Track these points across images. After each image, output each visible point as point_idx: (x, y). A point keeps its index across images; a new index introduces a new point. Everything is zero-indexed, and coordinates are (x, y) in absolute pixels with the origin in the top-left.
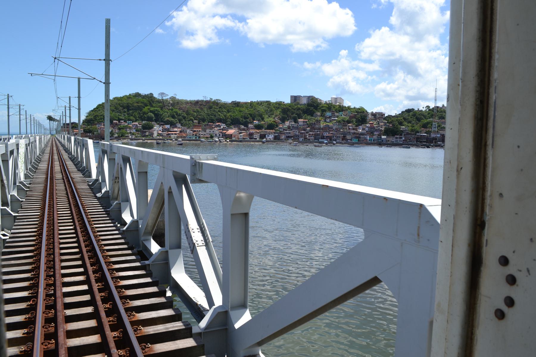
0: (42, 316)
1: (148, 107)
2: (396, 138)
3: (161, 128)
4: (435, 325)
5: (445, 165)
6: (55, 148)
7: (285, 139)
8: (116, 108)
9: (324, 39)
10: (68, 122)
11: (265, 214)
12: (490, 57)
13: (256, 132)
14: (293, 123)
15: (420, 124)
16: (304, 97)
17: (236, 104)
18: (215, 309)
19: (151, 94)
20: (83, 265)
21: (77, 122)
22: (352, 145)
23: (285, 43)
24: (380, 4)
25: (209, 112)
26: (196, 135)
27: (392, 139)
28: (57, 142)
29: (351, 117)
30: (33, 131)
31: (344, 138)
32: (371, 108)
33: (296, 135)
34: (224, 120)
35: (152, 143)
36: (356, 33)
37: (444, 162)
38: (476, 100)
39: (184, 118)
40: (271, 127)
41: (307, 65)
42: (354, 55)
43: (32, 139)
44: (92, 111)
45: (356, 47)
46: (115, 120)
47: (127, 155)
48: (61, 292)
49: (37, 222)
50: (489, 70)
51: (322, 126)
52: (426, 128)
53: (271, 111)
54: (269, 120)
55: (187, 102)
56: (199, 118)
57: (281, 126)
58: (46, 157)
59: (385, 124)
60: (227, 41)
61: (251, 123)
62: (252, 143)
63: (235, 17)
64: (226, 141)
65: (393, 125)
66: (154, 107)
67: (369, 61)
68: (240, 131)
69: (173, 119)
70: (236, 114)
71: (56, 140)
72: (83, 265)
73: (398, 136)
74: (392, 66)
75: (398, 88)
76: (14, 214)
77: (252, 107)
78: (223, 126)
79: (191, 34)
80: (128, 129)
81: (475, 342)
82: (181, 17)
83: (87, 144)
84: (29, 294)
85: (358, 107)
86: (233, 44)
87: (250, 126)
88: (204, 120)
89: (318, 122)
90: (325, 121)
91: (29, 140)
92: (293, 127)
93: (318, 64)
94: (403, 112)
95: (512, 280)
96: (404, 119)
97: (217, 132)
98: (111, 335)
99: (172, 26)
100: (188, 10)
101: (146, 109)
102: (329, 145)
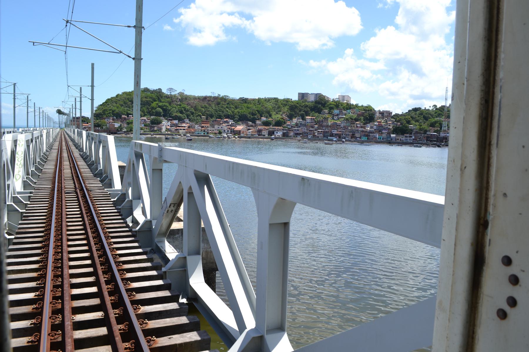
0: (49, 321)
1: (156, 102)
2: (406, 137)
3: (169, 123)
5: (448, 164)
6: (64, 143)
7: (294, 136)
8: (125, 103)
9: (330, 38)
10: (78, 115)
11: (306, 223)
12: (496, 56)
13: (265, 129)
14: (301, 120)
15: (428, 122)
16: (312, 94)
17: (244, 101)
18: (248, 332)
19: (160, 89)
20: (88, 244)
22: (362, 143)
23: (291, 41)
24: (386, 4)
25: (217, 108)
26: (204, 131)
27: (402, 138)
28: (67, 136)
29: (359, 115)
30: (41, 125)
31: (353, 136)
32: (378, 107)
33: (305, 133)
34: (231, 116)
35: (161, 138)
36: (362, 32)
37: (448, 161)
38: (481, 99)
39: (192, 113)
40: (279, 123)
41: (313, 63)
42: (359, 54)
43: (36, 134)
44: (101, 105)
45: (362, 46)
46: (124, 114)
47: (202, 170)
48: (69, 293)
49: (39, 245)
50: (495, 69)
51: (330, 124)
52: (434, 127)
53: (279, 107)
54: (277, 117)
55: (195, 98)
56: (207, 114)
57: (288, 123)
58: (54, 154)
59: (393, 123)
60: (234, 38)
61: (259, 119)
62: (261, 140)
63: (242, 15)
64: (234, 137)
65: (401, 124)
67: (374, 60)
68: (248, 128)
69: (181, 115)
70: (244, 110)
71: (65, 134)
72: (91, 258)
73: (408, 135)
74: (396, 65)
75: (402, 87)
76: (21, 211)
77: (260, 104)
78: (231, 122)
79: (198, 31)
81: (476, 342)
82: (188, 15)
84: (35, 296)
85: (365, 105)
86: (240, 41)
87: (258, 122)
88: (212, 116)
89: (326, 119)
90: (333, 119)
91: (33, 135)
92: (301, 124)
93: (324, 62)
94: (409, 111)
95: (514, 280)
96: (412, 117)
97: (226, 128)
98: (117, 328)
99: (180, 23)
100: (196, 7)
101: (154, 104)
102: (338, 142)
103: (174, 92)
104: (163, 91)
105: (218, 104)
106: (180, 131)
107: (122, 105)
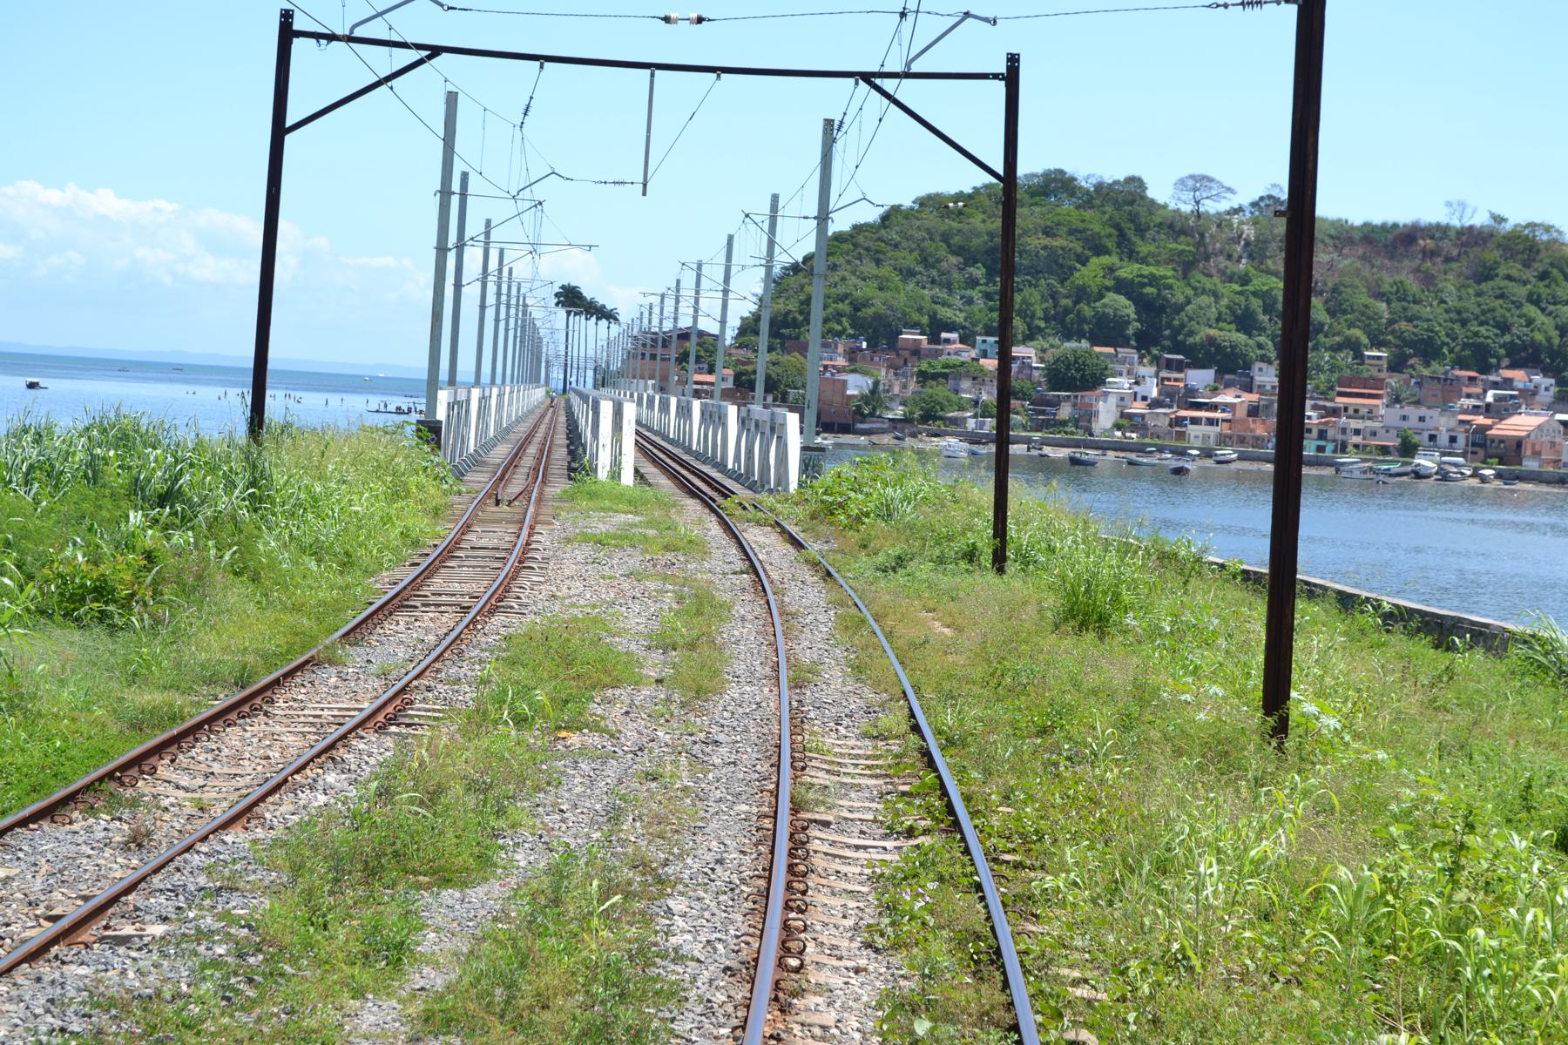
1: (1105, 260)
8: (924, 261)
19: (1136, 183)
25: (1471, 305)
56: (1399, 335)
64: (1475, 475)
66: (1144, 261)
69: (1241, 338)
80: (966, 384)
83: (783, 425)
88: (1428, 350)
101: (1091, 273)
103: (1216, 198)
104: (1150, 194)
105: (1485, 274)
106: (1192, 430)
107: (908, 274)
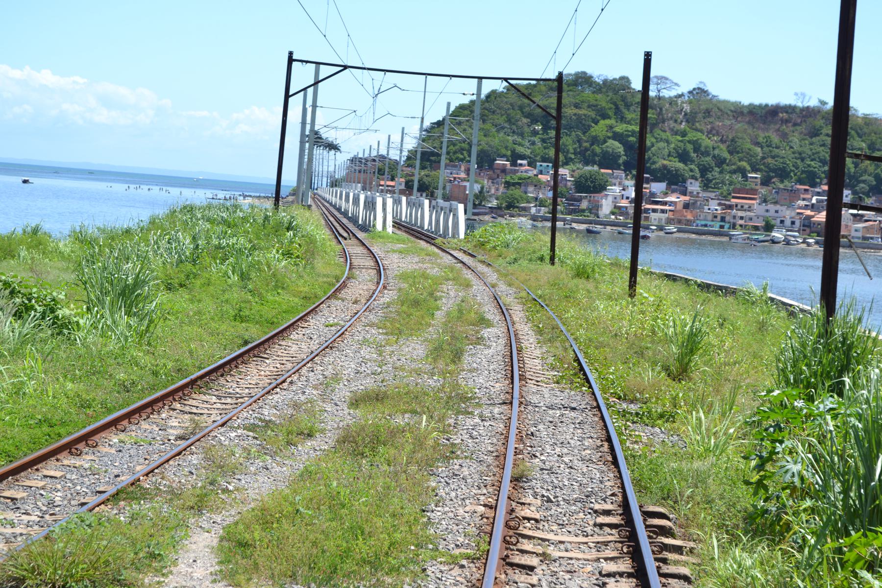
1: (608, 122)
4: (472, 259)
21: (398, 158)
25: (807, 150)
39: (720, 162)
55: (741, 113)
56: (767, 166)
69: (681, 165)
80: (531, 189)
88: (783, 174)
101: (600, 129)
